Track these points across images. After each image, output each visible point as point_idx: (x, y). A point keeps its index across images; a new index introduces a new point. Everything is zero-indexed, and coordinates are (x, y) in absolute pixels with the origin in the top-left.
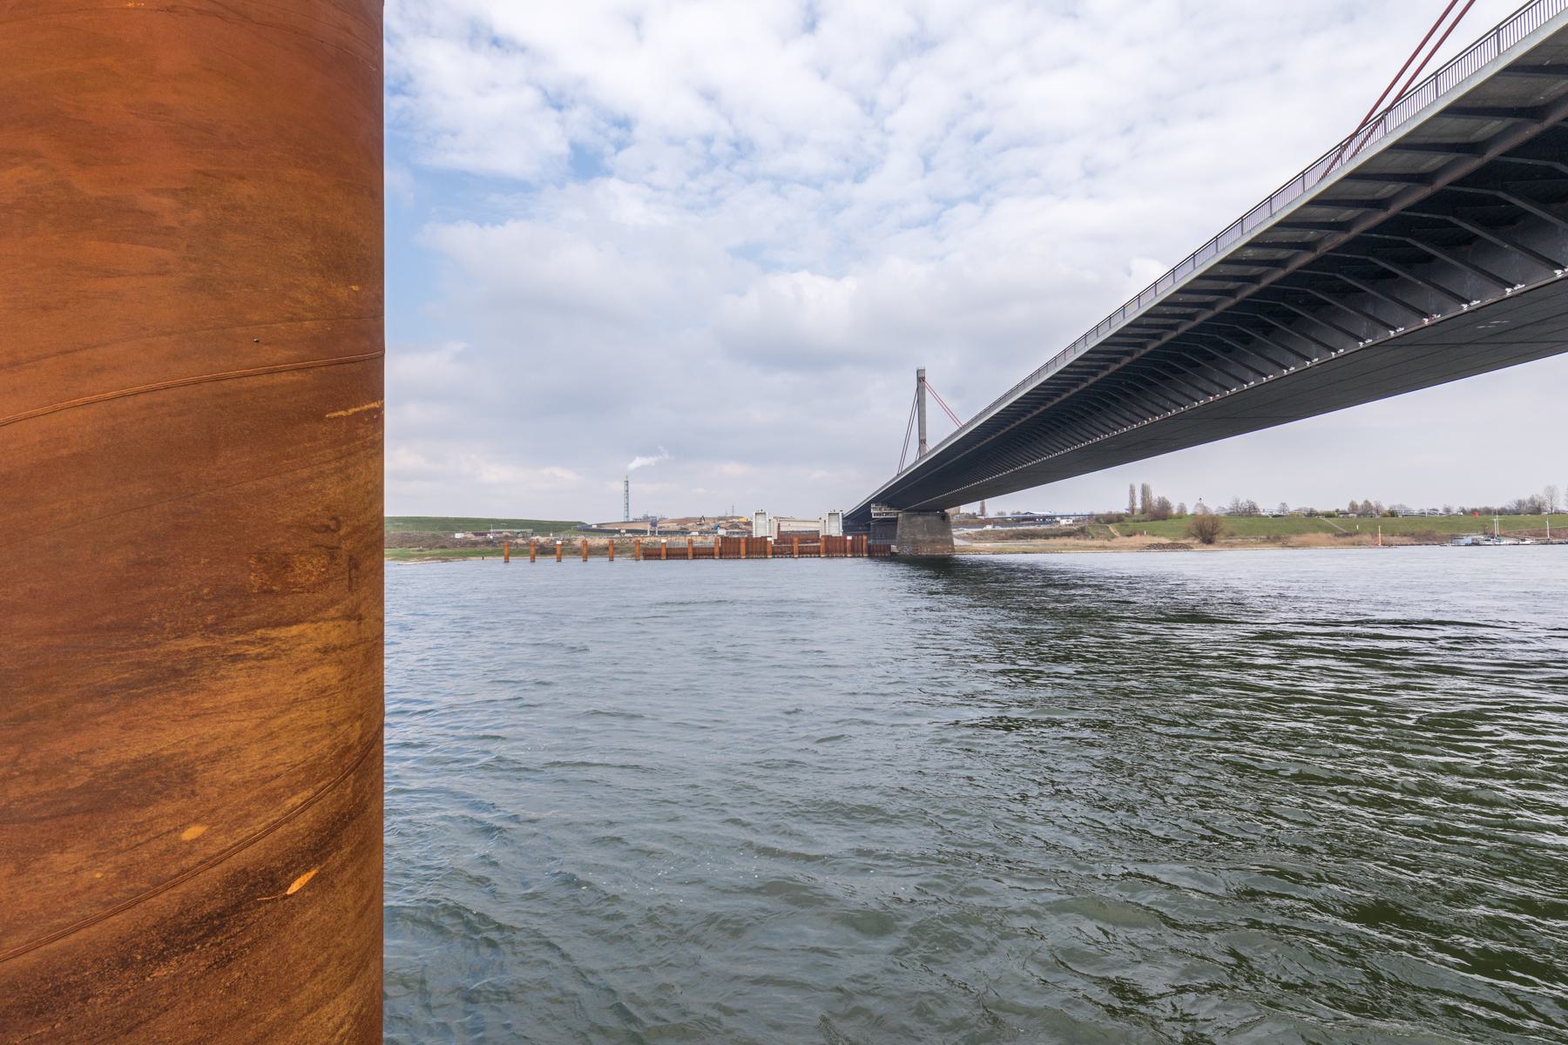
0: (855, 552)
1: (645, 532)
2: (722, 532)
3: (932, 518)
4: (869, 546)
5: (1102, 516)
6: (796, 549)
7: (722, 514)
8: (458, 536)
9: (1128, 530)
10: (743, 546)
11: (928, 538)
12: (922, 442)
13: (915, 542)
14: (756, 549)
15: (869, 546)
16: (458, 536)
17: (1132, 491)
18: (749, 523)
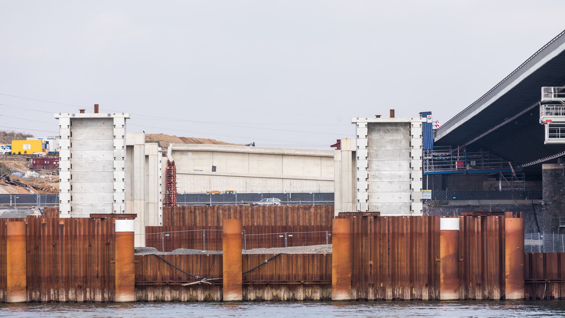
0: (472, 278)
4: (528, 258)
6: (231, 268)
15: (528, 258)
18: (48, 162)
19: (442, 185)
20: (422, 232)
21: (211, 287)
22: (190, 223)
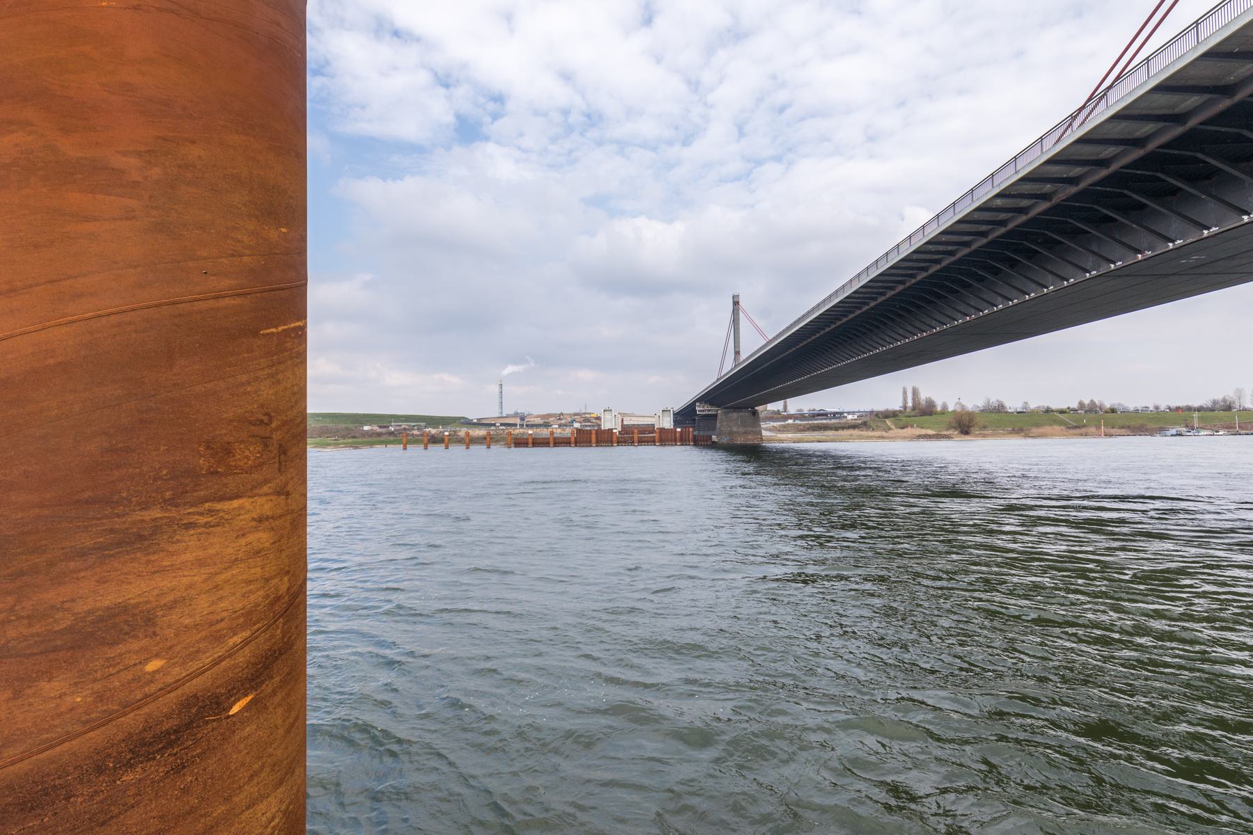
0: (683, 441)
1: (515, 425)
2: (577, 425)
3: (745, 414)
4: (694, 437)
5: (881, 412)
6: (636, 439)
7: (577, 411)
8: (366, 428)
9: (901, 424)
10: (594, 436)
11: (742, 430)
12: (737, 353)
13: (731, 433)
14: (604, 438)
15: (694, 437)
16: (366, 428)
17: (905, 393)
18: (598, 418)
19: (677, 422)
20: (673, 431)
21: (632, 443)
22: (626, 430)
